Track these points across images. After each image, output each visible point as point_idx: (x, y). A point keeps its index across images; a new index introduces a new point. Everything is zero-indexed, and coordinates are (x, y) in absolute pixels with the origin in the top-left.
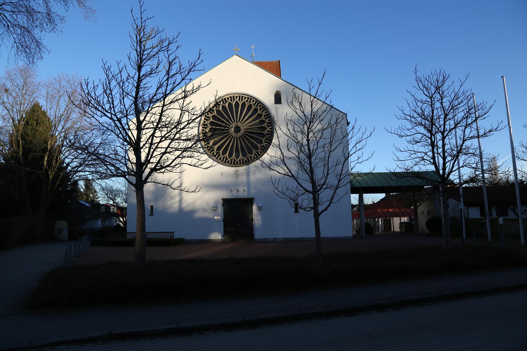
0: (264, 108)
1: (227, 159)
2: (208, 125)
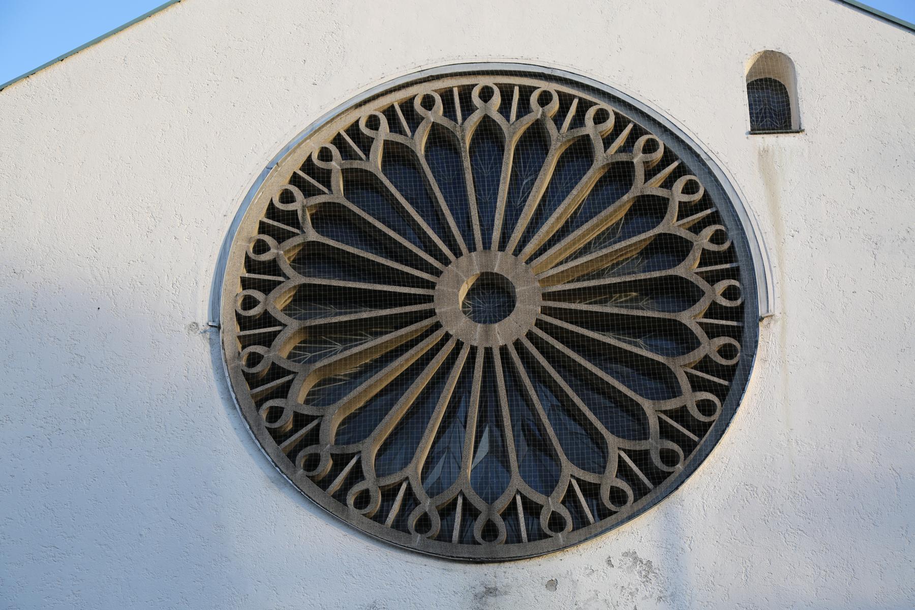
0: (679, 159)
1: (410, 500)
2: (285, 265)
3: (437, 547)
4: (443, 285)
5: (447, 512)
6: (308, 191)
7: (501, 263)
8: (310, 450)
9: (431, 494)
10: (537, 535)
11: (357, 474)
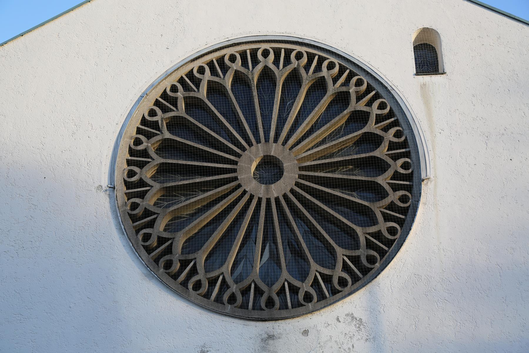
0: (375, 89)
1: (225, 285)
2: (152, 152)
3: (240, 312)
4: (242, 163)
5: (245, 292)
6: (165, 110)
7: (275, 150)
8: (167, 257)
9: (236, 282)
10: (297, 305)
11: (194, 271)
